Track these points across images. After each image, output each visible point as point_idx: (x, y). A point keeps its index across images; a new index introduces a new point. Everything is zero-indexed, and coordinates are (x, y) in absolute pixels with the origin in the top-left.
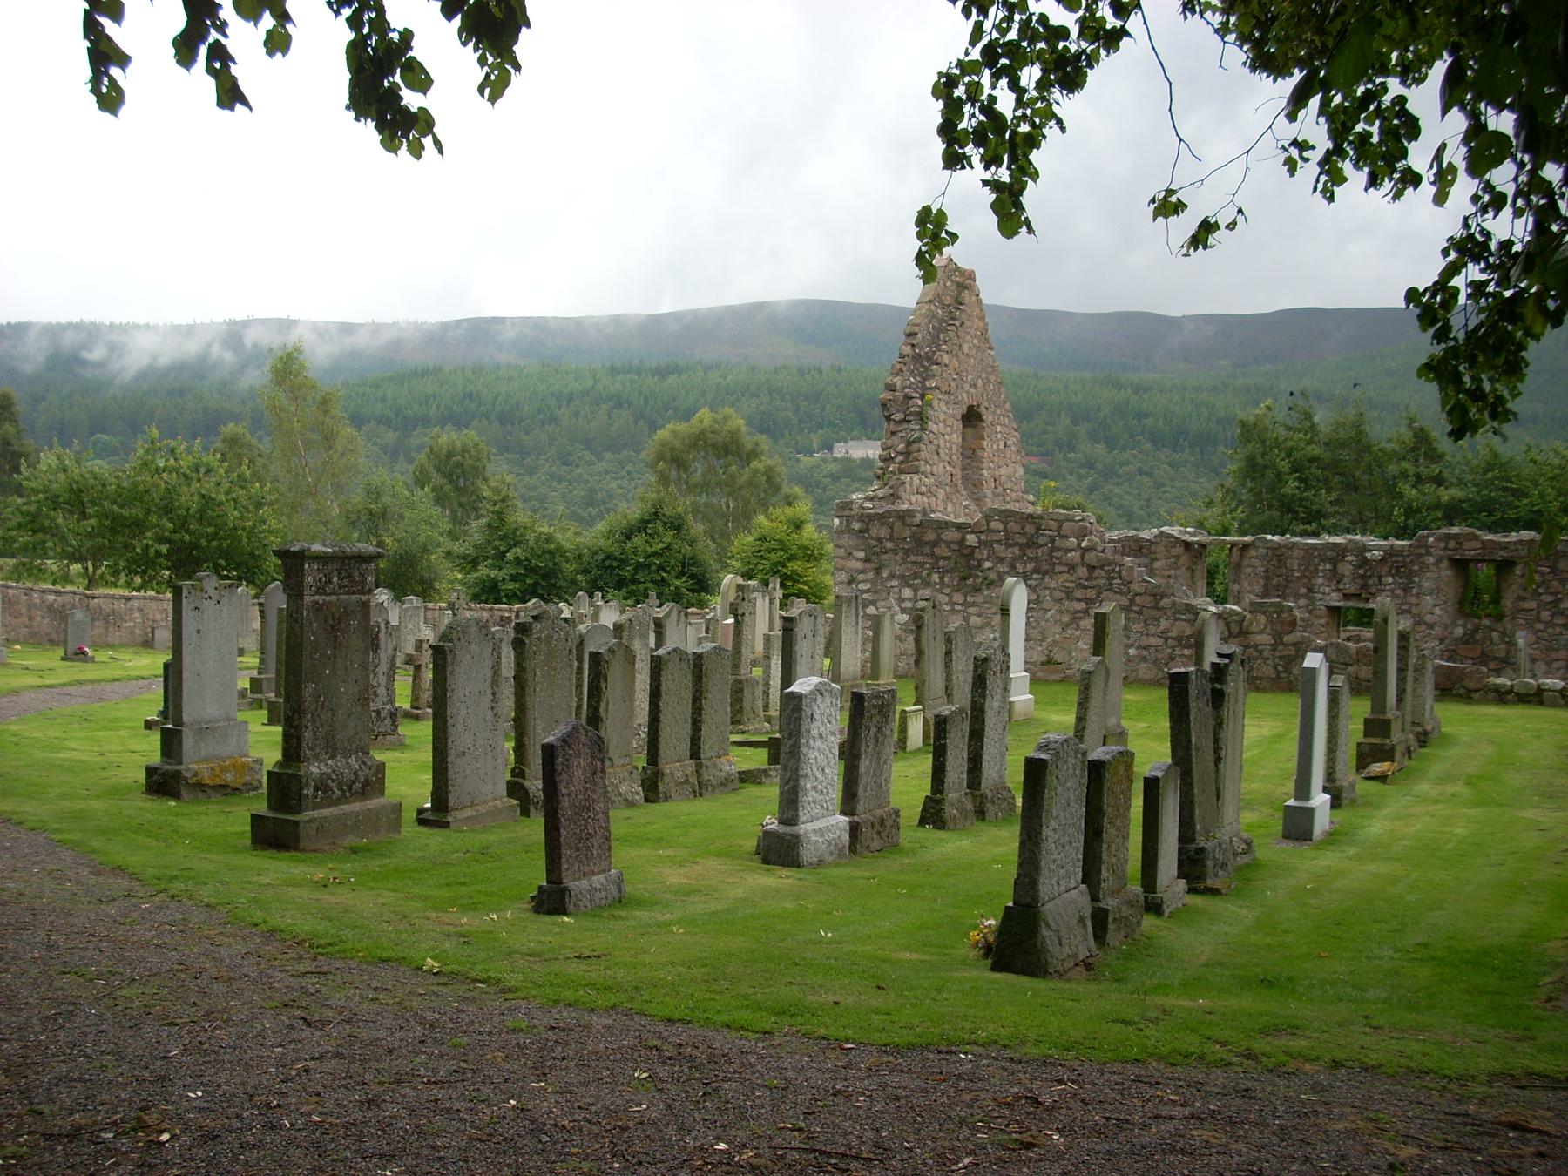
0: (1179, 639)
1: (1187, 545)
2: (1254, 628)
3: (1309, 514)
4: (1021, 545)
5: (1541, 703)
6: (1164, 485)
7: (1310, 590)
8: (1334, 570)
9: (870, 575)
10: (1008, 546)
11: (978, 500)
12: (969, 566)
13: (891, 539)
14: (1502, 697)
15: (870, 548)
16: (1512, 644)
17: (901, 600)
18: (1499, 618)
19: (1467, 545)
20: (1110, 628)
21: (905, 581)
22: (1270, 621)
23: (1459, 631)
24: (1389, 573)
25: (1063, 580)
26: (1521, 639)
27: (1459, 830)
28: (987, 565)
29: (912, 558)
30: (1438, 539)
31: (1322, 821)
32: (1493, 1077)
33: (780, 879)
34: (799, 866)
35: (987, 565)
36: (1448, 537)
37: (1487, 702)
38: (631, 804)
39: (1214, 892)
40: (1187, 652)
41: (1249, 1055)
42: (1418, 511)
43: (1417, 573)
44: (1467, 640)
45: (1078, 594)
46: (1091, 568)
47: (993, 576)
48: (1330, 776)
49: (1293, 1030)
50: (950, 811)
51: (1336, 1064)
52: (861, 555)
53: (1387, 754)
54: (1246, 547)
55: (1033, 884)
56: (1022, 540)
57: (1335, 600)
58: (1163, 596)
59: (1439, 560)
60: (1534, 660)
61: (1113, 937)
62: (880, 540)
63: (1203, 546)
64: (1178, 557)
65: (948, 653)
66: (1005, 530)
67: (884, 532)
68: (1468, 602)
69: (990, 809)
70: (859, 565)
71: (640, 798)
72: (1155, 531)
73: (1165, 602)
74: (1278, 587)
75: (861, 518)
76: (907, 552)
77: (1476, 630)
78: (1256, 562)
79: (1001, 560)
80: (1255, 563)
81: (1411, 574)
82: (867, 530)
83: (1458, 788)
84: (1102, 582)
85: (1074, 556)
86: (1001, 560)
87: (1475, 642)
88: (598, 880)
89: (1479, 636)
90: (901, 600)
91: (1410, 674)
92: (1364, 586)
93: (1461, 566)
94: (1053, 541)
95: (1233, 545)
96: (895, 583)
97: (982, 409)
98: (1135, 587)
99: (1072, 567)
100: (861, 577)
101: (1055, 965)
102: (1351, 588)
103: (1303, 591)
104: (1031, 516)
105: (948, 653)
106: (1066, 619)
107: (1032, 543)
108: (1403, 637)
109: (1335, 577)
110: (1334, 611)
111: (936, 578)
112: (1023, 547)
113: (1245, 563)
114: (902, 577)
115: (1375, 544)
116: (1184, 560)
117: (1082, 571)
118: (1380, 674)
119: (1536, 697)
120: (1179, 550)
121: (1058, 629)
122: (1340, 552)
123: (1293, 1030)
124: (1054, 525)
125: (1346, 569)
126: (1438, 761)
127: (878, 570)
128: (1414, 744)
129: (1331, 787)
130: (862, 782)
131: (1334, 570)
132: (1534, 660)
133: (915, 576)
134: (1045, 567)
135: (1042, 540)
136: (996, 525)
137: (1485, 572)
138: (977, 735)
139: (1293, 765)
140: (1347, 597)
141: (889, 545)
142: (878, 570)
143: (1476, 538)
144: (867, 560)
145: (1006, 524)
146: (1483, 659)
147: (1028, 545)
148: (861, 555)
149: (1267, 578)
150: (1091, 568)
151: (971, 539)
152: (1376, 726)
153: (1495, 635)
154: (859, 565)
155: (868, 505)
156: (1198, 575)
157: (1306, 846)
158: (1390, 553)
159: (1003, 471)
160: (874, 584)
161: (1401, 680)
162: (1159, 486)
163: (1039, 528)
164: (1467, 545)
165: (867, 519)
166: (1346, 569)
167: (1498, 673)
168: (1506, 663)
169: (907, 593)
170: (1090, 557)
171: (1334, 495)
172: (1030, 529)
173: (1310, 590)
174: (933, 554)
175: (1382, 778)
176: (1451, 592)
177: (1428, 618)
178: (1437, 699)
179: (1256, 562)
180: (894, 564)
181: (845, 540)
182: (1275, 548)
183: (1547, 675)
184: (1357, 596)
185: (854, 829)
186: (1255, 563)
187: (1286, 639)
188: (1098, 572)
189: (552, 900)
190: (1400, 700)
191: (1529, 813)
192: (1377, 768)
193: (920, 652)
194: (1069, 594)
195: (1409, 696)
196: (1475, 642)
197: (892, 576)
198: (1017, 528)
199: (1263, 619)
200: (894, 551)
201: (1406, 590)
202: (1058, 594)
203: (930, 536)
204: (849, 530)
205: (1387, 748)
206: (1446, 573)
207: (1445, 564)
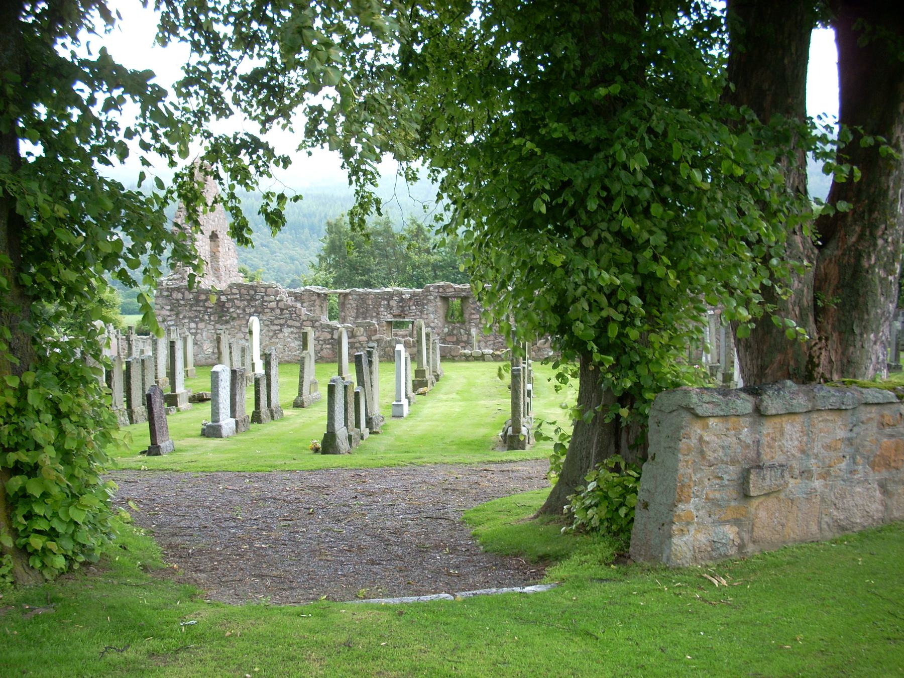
0: (324, 341)
1: (319, 294)
2: (358, 334)
3: (363, 271)
4: (247, 300)
5: (484, 360)
6: (275, 252)
7: (378, 314)
8: (388, 304)
9: (174, 317)
10: (241, 300)
11: (218, 277)
12: (223, 311)
13: (183, 299)
14: (468, 358)
15: (173, 304)
16: (469, 334)
17: (190, 329)
18: (463, 323)
19: (448, 290)
20: (309, 338)
21: (191, 319)
22: (366, 330)
23: (446, 330)
24: (414, 305)
25: (268, 316)
26: (474, 331)
27: (457, 410)
28: (232, 310)
29: (195, 308)
30: (435, 287)
31: (406, 410)
32: (478, 462)
33: (213, 442)
34: (221, 437)
35: (232, 310)
36: (439, 287)
37: (461, 361)
38: (126, 425)
39: (377, 433)
40: (328, 346)
41: (411, 463)
42: (418, 267)
43: (426, 304)
44: (450, 334)
45: (276, 322)
46: (282, 310)
47: (235, 315)
48: (406, 395)
49: (421, 458)
50: (263, 416)
51: (436, 463)
52: (169, 308)
53: (425, 384)
54: (346, 295)
55: (333, 425)
56: (248, 298)
57: (390, 318)
58: (316, 321)
59: (436, 298)
60: (479, 342)
61: (354, 445)
62: (177, 300)
63: (326, 295)
64: (315, 301)
65: (231, 353)
66: (240, 293)
67: (180, 296)
68: (449, 316)
69: (275, 415)
70: (168, 313)
71: (128, 422)
72: (302, 289)
73: (317, 324)
74: (363, 313)
75: (167, 290)
76: (191, 306)
77: (454, 328)
78: (352, 302)
79: (238, 308)
80: (352, 303)
81: (423, 304)
82: (171, 295)
83: (454, 396)
84: (287, 316)
85: (273, 305)
86: (238, 308)
87: (454, 335)
88: (167, 443)
89: (455, 332)
90: (190, 329)
91: (431, 350)
92: (403, 311)
93: (445, 299)
94: (263, 297)
95: (340, 294)
96: (186, 321)
97: (218, 233)
98: (303, 317)
99: (272, 309)
100: (169, 318)
101: (342, 451)
102: (396, 312)
103: (375, 314)
104: (252, 286)
105: (231, 353)
106: (271, 334)
107: (253, 299)
108: (428, 335)
109: (389, 307)
110: (390, 323)
111: (206, 317)
112: (249, 301)
113: (346, 302)
114: (190, 318)
115: (407, 291)
116: (318, 302)
117: (278, 311)
118: (420, 352)
119: (482, 358)
120: (315, 297)
121: (268, 339)
122: (391, 296)
123: (421, 458)
124: (263, 290)
125: (393, 303)
126: (444, 386)
127: (177, 315)
128: (434, 380)
129: (407, 396)
130: (238, 404)
131: (388, 304)
132: (479, 342)
133: (196, 317)
134: (260, 310)
135: (257, 297)
136: (235, 291)
137: (457, 302)
138: (269, 386)
139: (394, 388)
140: (395, 316)
141: (182, 302)
142: (177, 315)
143: (452, 287)
144: (171, 310)
145: (240, 291)
146: (457, 342)
147: (251, 300)
148: (169, 308)
149: (357, 309)
150: (282, 310)
151: (223, 298)
152: (420, 373)
153: (462, 331)
154: (168, 313)
155: (170, 283)
156: (324, 309)
157: (402, 419)
158: (414, 295)
159: (228, 262)
160: (176, 322)
161: (428, 353)
162: (273, 253)
163: (256, 292)
164: (448, 290)
165: (171, 290)
166: (393, 303)
167: (464, 348)
168: (468, 343)
169: (193, 325)
170: (281, 305)
171: (377, 260)
172: (252, 292)
173: (378, 314)
174: (204, 306)
175: (424, 394)
176: (441, 312)
177: (432, 325)
178: (444, 358)
179: (352, 302)
180: (185, 312)
181: (160, 301)
182: (360, 295)
183: (486, 347)
184: (400, 316)
185: (237, 422)
186: (352, 303)
187: (373, 338)
188: (285, 311)
189: (154, 450)
190: (428, 362)
191: (482, 402)
192: (421, 390)
193: (220, 353)
194: (272, 322)
195: (431, 360)
196: (454, 335)
197: (184, 317)
198: (245, 292)
199: (362, 329)
200: (185, 305)
201: (421, 312)
202: (266, 323)
203: (203, 297)
204: (162, 296)
205: (614, 270)
206: (439, 303)
207: (438, 299)
